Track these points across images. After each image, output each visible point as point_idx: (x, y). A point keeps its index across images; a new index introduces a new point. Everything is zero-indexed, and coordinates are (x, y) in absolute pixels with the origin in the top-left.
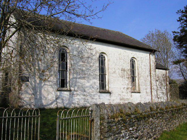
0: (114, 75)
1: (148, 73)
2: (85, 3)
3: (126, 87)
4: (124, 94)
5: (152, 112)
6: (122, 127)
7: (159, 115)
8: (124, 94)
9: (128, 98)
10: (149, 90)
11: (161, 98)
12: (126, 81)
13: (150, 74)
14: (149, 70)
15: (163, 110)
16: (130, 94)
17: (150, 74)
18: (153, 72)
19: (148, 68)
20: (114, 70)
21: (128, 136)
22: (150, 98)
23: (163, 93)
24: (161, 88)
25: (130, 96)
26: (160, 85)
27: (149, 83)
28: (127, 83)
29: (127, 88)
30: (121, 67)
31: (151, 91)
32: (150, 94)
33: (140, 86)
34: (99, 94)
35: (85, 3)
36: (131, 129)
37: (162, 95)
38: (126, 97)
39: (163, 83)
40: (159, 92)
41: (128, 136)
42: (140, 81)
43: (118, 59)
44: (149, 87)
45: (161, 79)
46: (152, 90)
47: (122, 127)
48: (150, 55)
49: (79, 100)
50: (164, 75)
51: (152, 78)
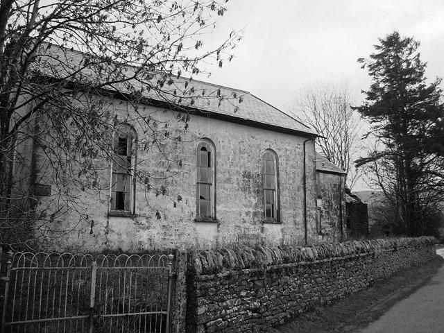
0: (226, 186)
1: (299, 182)
2: (141, 34)
3: (251, 210)
4: (247, 225)
5: (289, 265)
6: (226, 289)
7: (301, 270)
8: (247, 225)
9: (256, 233)
10: (300, 219)
11: (328, 234)
12: (252, 199)
13: (304, 184)
14: (301, 176)
15: (312, 260)
16: (258, 226)
17: (304, 184)
18: (309, 182)
19: (300, 171)
20: (228, 176)
21: (237, 305)
22: (303, 234)
23: (332, 224)
24: (328, 213)
25: (259, 231)
26: (326, 207)
27: (300, 204)
28: (254, 203)
29: (255, 214)
30: (243, 169)
31: (305, 219)
32: (301, 226)
33: (283, 210)
34: (194, 225)
35: (141, 34)
36: (243, 294)
37: (330, 229)
38: (251, 233)
39: (333, 202)
40: (324, 223)
41: (237, 305)
42: (283, 200)
43: (238, 151)
44: (301, 212)
45: (330, 194)
46: (308, 218)
47: (226, 289)
48: (304, 145)
49: (150, 235)
50: (335, 185)
51: (308, 193)
